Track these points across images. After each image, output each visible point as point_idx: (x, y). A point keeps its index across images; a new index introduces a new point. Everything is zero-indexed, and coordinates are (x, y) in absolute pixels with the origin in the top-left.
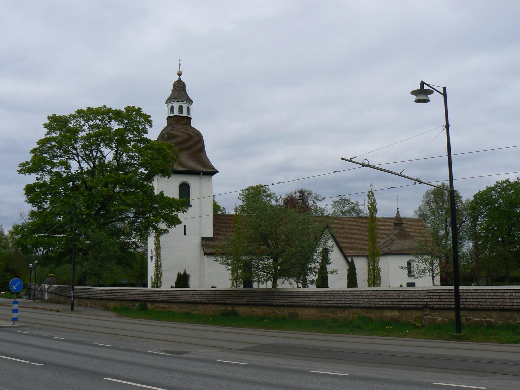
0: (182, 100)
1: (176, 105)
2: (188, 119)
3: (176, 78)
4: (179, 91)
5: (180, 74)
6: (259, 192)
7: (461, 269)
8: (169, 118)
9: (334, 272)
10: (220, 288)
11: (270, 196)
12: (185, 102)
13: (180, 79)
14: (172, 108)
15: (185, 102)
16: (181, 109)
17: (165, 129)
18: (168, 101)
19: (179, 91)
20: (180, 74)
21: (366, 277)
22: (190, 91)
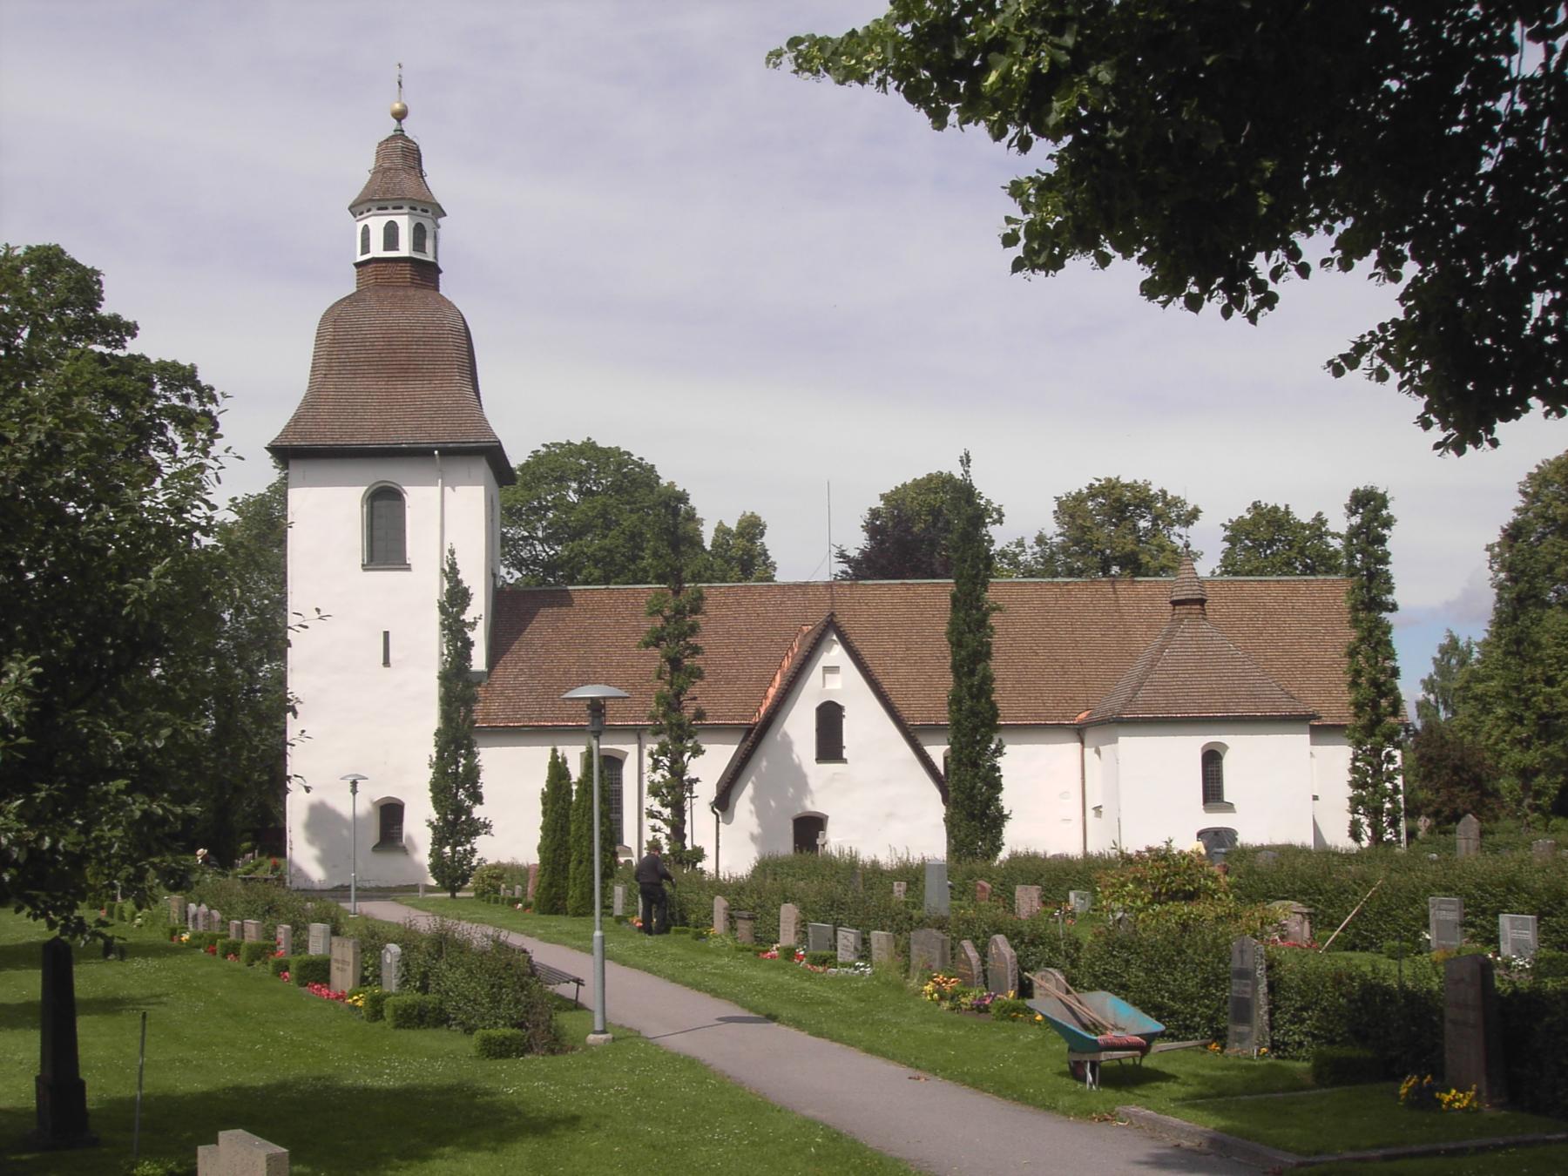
1: (377, 224)
13: (400, 134)
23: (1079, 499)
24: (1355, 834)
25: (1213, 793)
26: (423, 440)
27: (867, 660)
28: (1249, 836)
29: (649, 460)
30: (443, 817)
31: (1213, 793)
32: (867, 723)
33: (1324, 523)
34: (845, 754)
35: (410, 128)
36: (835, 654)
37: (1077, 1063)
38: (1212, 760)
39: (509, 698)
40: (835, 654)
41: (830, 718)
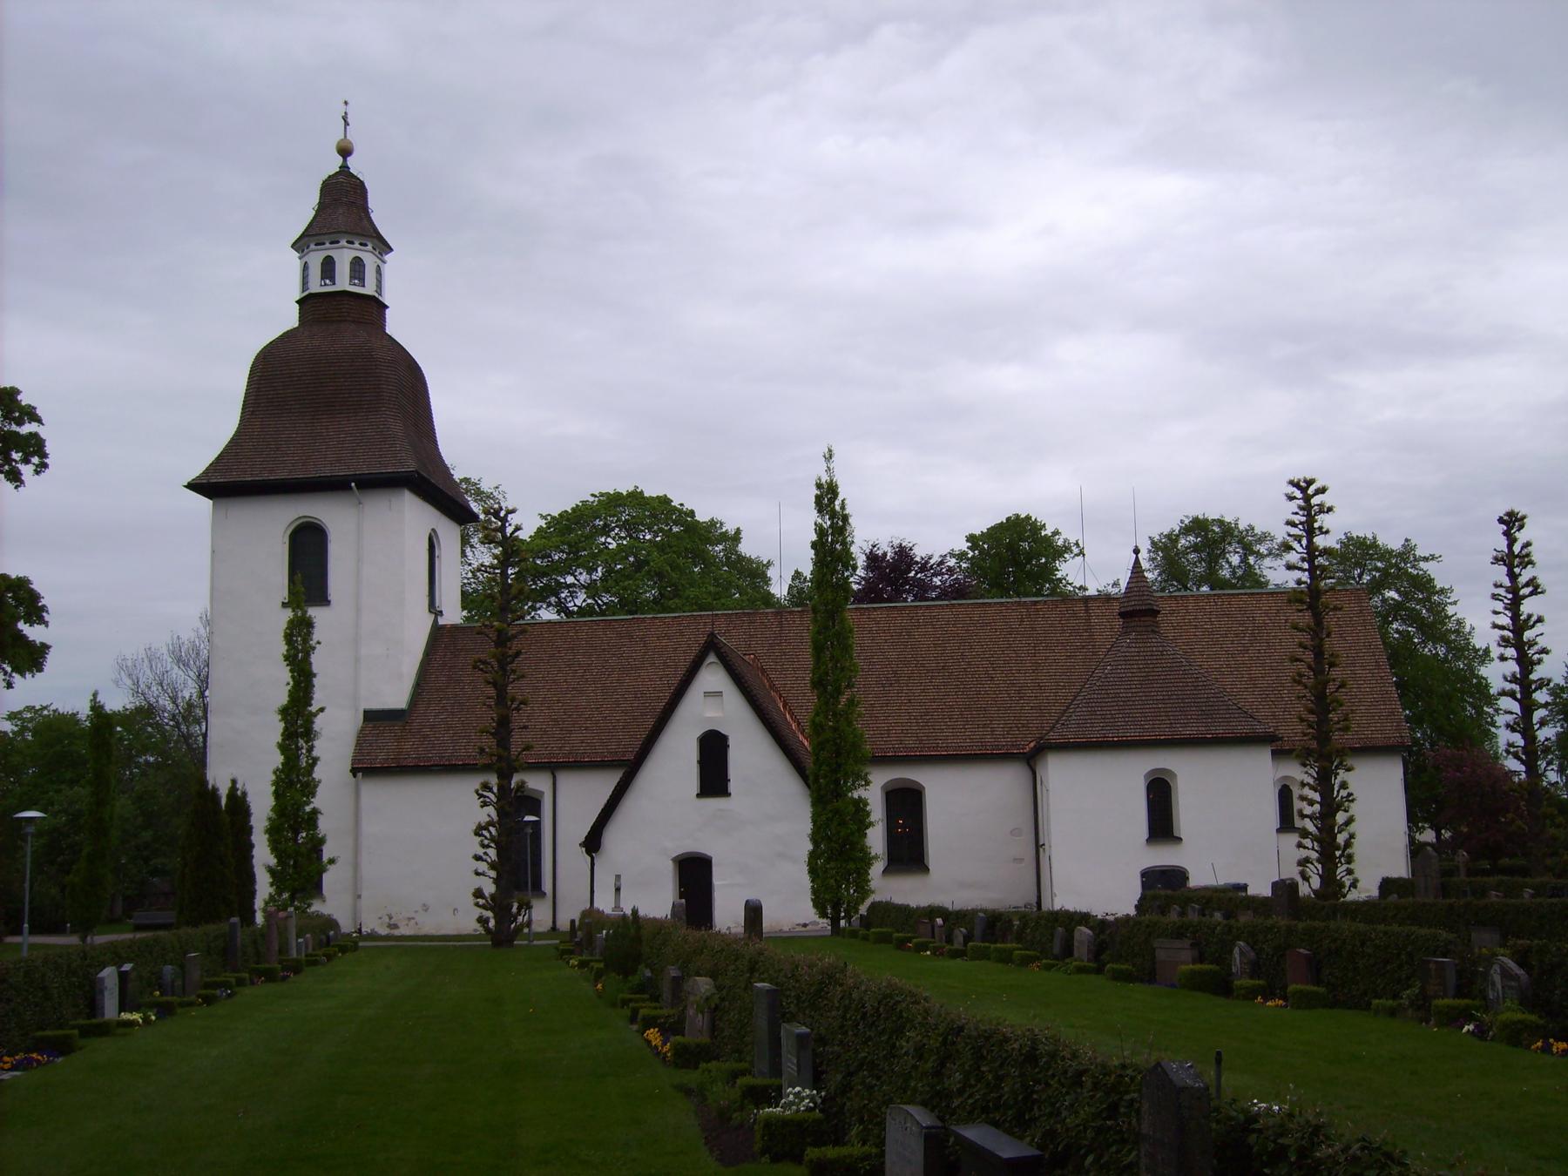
0: (334, 237)
1: (316, 259)
2: (375, 307)
3: (333, 164)
4: (343, 209)
5: (345, 152)
6: (1013, 548)
7: (559, 924)
8: (307, 303)
9: (332, 861)
10: (1395, 875)
11: (924, 566)
12: (343, 243)
13: (345, 168)
14: (328, 268)
15: (343, 243)
16: (357, 267)
17: (287, 337)
18: (300, 245)
19: (343, 209)
20: (345, 152)
21: (898, 900)
22: (381, 213)
23: (1172, 538)
24: (906, 805)
25: (1161, 825)
26: (342, 471)
27: (682, 671)
28: (1199, 878)
29: (688, 506)
30: (280, 862)
31: (1161, 825)
32: (753, 756)
33: (1413, 548)
34: (732, 787)
35: (355, 165)
36: (712, 677)
37: (94, 1016)
38: (1160, 795)
39: (425, 737)
40: (712, 677)
41: (713, 749)
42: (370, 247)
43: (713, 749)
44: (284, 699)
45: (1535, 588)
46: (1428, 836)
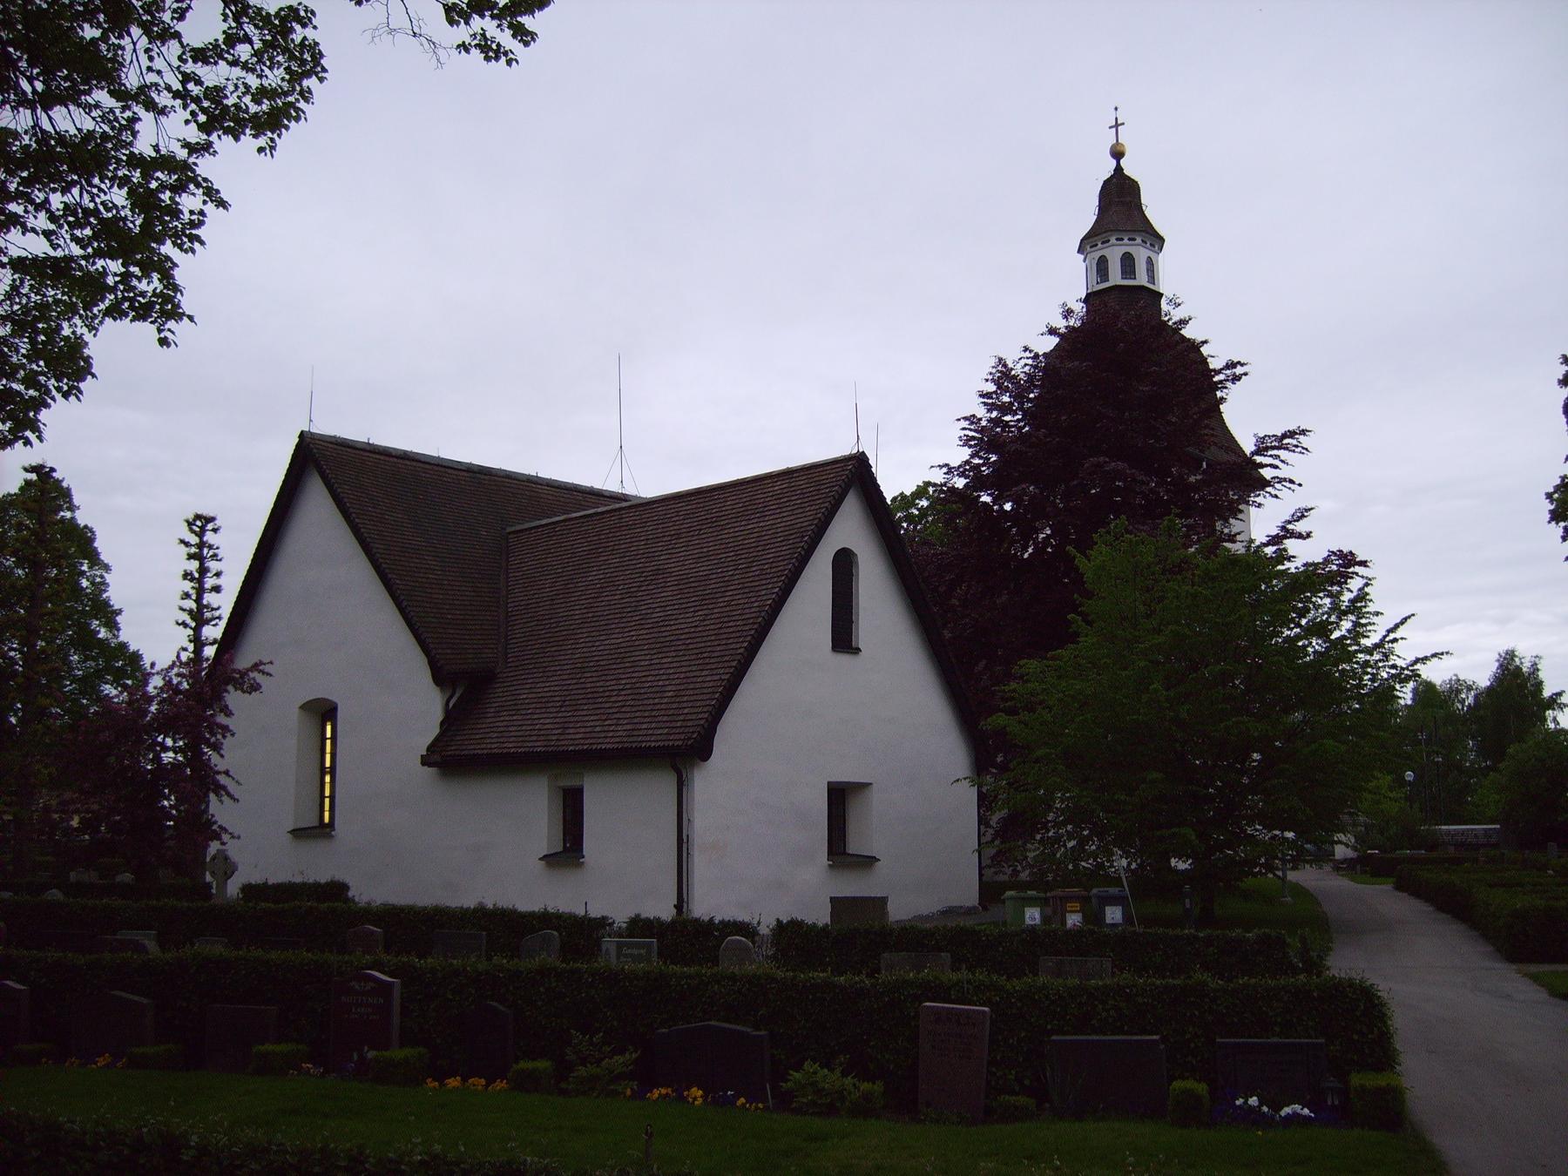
1: (1114, 254)
4: (1121, 204)
5: (1117, 154)
13: (1119, 169)
14: (1102, 267)
18: (1087, 243)
19: (1121, 204)
20: (1117, 154)
35: (1129, 168)
41: (844, 563)
42: (1139, 240)
43: (844, 563)
44: (176, 272)
45: (187, 575)
46: (68, 515)
